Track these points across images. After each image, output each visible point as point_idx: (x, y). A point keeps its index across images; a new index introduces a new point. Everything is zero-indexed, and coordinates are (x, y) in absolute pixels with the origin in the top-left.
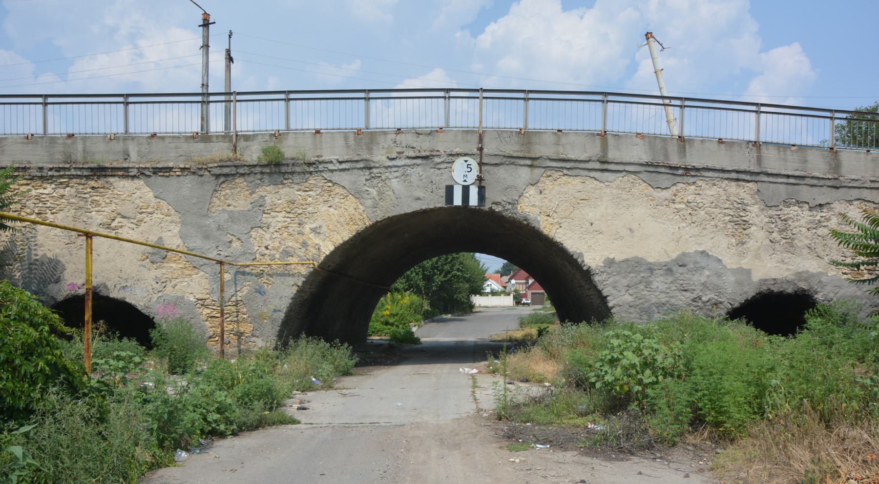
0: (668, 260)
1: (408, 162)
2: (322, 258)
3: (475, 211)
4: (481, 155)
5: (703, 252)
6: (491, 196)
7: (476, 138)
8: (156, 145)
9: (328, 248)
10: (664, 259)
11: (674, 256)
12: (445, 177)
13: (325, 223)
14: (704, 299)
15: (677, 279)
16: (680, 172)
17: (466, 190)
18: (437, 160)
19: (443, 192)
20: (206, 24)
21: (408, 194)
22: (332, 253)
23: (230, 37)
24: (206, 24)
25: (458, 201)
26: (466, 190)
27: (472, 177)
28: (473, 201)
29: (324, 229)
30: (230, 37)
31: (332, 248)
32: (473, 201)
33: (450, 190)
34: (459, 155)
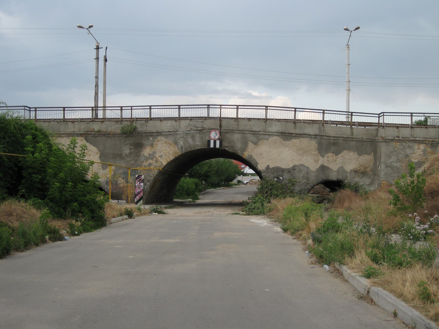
0: (289, 167)
1: (194, 132)
2: (163, 166)
3: (218, 149)
4: (221, 129)
5: (302, 165)
6: (225, 144)
7: (218, 122)
8: (251, 123)
9: (165, 163)
10: (288, 167)
11: (291, 166)
12: (207, 137)
13: (163, 153)
14: (303, 182)
15: (292, 175)
16: (313, 137)
17: (215, 142)
18: (205, 131)
19: (206, 143)
20: (98, 48)
21: (197, 143)
22: (167, 165)
23: (106, 49)
24: (98, 48)
25: (212, 146)
26: (215, 142)
27: (217, 137)
28: (218, 146)
29: (163, 156)
30: (106, 49)
31: (166, 163)
32: (218, 146)
33: (209, 142)
34: (213, 129)
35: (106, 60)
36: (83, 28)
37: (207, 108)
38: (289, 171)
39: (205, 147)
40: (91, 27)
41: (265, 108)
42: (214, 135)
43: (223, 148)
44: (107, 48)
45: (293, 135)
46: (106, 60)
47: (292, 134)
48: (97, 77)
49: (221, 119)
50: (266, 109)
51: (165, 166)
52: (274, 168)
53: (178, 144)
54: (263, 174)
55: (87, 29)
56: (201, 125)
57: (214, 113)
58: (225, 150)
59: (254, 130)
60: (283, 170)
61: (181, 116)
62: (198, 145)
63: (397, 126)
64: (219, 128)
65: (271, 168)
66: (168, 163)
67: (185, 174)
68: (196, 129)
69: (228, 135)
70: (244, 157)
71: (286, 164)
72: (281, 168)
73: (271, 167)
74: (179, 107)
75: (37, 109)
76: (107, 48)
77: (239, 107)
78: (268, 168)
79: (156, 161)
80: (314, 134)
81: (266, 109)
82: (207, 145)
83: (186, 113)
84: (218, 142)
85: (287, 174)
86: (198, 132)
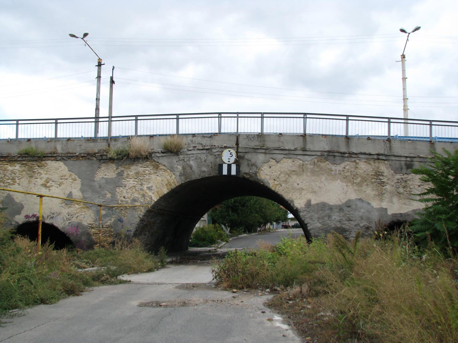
0: (340, 203)
1: (199, 152)
2: (153, 202)
9: (155, 199)
11: (344, 201)
13: (154, 185)
15: (346, 214)
17: (229, 166)
20: (100, 65)
22: (158, 201)
23: (113, 69)
24: (100, 65)
25: (225, 172)
26: (229, 166)
27: (232, 160)
28: (234, 172)
29: (154, 188)
30: (113, 69)
31: (158, 198)
32: (234, 172)
33: (221, 167)
34: (226, 147)
35: (112, 82)
36: (77, 38)
38: (340, 209)
39: (214, 173)
40: (86, 35)
41: (302, 116)
42: (228, 157)
43: (241, 176)
44: (114, 67)
45: (347, 155)
46: (112, 82)
47: (345, 153)
48: (98, 99)
49: (237, 136)
51: (157, 203)
52: (317, 204)
53: (175, 170)
54: (301, 214)
55: (82, 39)
56: (210, 144)
57: (229, 126)
58: (244, 178)
59: (287, 148)
60: (331, 208)
62: (204, 172)
64: (235, 145)
65: (314, 205)
66: (161, 198)
67: (262, 185)
68: (201, 148)
69: (247, 156)
71: (406, 212)
72: (329, 205)
73: (313, 202)
74: (178, 117)
76: (114, 67)
78: (308, 204)
79: (144, 196)
80: (377, 153)
82: (217, 172)
85: (337, 214)
86: (204, 151)
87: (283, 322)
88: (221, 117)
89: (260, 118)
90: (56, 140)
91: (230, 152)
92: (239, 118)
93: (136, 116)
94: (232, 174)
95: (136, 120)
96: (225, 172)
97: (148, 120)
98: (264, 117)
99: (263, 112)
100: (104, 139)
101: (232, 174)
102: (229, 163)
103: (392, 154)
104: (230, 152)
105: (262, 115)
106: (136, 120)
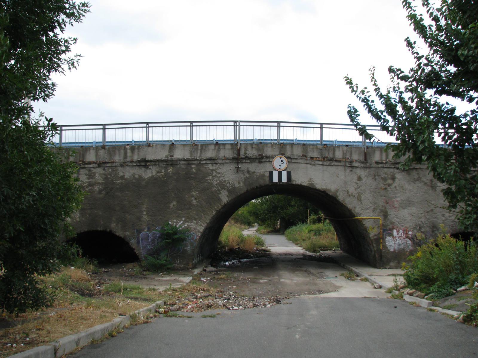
3: (284, 185)
6: (294, 177)
17: (280, 174)
25: (276, 179)
26: (280, 174)
27: (284, 167)
28: (284, 179)
32: (284, 179)
33: (271, 173)
37: (190, 126)
41: (145, 125)
50: (278, 126)
61: (63, 141)
63: (172, 145)
70: (242, 192)
75: (324, 126)
77: (107, 127)
81: (278, 126)
83: (131, 135)
84: (284, 174)
87: (411, 289)
88: (149, 127)
89: (145, 128)
90: (149, 144)
91: (282, 159)
92: (241, 127)
93: (104, 125)
94: (274, 181)
95: (191, 126)
96: (276, 179)
97: (133, 129)
98: (280, 126)
99: (104, 123)
100: (184, 145)
101: (274, 181)
102: (280, 170)
103: (225, 198)
104: (282, 159)
105: (278, 124)
106: (104, 129)
